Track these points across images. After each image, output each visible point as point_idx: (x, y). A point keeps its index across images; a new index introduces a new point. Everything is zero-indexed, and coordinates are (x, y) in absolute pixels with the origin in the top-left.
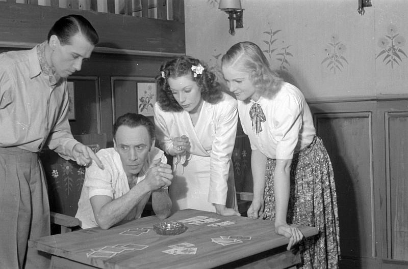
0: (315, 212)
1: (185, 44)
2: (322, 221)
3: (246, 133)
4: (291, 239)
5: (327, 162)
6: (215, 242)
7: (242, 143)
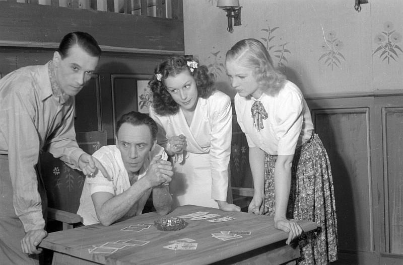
0: (316, 205)
1: (184, 42)
2: (323, 214)
3: (244, 131)
4: (291, 234)
5: (325, 156)
6: (215, 237)
7: (239, 139)
